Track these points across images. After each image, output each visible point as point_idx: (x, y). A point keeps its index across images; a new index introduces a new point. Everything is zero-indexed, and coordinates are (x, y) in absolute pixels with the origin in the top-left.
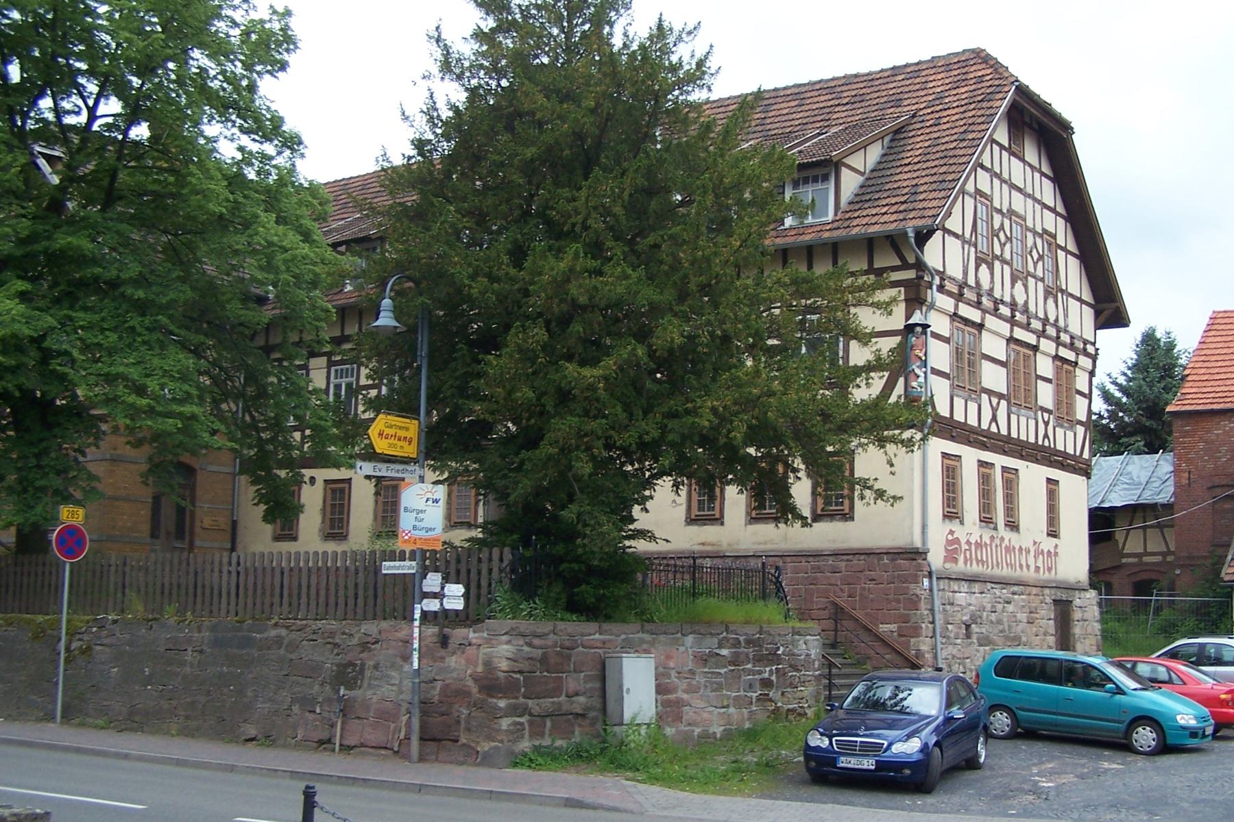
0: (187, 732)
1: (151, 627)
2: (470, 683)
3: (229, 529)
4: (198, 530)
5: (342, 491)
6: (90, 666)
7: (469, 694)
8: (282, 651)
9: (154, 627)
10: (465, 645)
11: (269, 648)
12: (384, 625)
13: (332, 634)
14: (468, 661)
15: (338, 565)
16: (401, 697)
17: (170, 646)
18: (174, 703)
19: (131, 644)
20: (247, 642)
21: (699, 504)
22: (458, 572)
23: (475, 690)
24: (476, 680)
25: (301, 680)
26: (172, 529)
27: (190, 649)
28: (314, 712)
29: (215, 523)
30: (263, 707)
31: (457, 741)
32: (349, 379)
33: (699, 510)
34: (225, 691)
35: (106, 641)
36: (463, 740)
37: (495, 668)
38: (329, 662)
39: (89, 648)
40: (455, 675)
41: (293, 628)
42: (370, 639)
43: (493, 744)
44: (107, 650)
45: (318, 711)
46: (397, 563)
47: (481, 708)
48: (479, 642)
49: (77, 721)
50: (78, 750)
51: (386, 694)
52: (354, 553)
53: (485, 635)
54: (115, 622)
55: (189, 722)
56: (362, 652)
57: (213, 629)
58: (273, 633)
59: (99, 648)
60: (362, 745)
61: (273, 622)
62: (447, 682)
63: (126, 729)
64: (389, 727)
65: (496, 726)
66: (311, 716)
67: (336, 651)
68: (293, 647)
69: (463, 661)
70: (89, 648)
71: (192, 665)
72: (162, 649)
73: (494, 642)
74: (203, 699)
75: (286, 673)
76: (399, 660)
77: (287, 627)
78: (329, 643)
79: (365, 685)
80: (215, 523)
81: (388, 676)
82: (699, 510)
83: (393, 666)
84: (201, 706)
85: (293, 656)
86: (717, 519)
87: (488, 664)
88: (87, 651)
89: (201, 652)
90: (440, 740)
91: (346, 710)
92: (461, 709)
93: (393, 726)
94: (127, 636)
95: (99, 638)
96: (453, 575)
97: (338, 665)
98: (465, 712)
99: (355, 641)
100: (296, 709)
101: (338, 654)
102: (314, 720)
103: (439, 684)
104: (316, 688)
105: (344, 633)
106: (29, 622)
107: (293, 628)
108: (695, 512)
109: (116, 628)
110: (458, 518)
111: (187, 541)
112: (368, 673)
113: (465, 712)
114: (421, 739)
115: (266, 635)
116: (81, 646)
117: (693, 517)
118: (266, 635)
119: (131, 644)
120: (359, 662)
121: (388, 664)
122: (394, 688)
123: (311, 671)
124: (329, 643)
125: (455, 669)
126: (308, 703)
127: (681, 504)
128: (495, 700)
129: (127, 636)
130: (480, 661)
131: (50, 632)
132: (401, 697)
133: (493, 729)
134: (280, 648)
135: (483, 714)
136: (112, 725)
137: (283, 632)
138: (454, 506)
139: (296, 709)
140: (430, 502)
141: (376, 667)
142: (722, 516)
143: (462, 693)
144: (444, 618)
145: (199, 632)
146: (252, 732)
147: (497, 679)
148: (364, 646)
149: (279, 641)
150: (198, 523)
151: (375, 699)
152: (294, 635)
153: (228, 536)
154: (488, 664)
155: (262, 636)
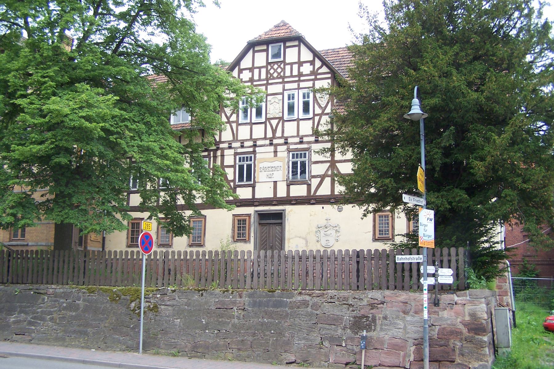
0: (60, 341)
1: (202, 294)
2: (461, 327)
3: (101, 241)
4: (89, 241)
5: (245, 220)
6: (157, 318)
7: (461, 333)
8: (309, 309)
9: (204, 294)
10: (452, 304)
11: (298, 308)
12: (387, 293)
13: (346, 299)
14: (457, 314)
15: (246, 258)
16: (407, 336)
17: (219, 306)
18: (228, 341)
19: (188, 305)
20: (279, 304)
21: (131, 239)
22: (449, 261)
23: (465, 331)
24: (465, 325)
25: (327, 327)
26: (77, 241)
27: (235, 308)
28: (341, 346)
29: (96, 238)
30: (299, 343)
31: (454, 362)
32: (303, 159)
33: (131, 242)
34: (268, 333)
35: (168, 303)
36: (458, 360)
37: (480, 318)
38: (347, 316)
39: (156, 307)
40: (449, 322)
41: (314, 295)
42: (376, 301)
43: (481, 363)
44: (170, 308)
45: (344, 345)
46: (408, 256)
47: (470, 341)
48: (464, 302)
49: (152, 351)
50: (84, 362)
51: (395, 334)
52: (210, 252)
53: (468, 298)
54: (174, 291)
55: (241, 353)
56: (372, 309)
57: (250, 296)
58: (300, 298)
59: (163, 307)
60: (380, 365)
61: (298, 291)
62: (443, 326)
63: (195, 357)
64: (400, 354)
65: (483, 352)
66: (339, 348)
67: (351, 309)
68: (316, 306)
69: (453, 314)
70: (156, 307)
71: (238, 318)
72: (213, 308)
73: (477, 302)
74: (250, 338)
75: (314, 322)
76: (401, 313)
77: (310, 295)
78: (345, 304)
79: (378, 328)
80: (96, 238)
81: (395, 323)
82: (131, 242)
83: (397, 317)
84: (249, 343)
85: (318, 312)
86: (390, 239)
87: (473, 315)
88: (155, 308)
89: (244, 309)
90: (440, 361)
91: (368, 344)
92: (456, 342)
93: (402, 353)
94: (186, 300)
95: (164, 301)
96: (445, 262)
97: (355, 317)
98: (459, 344)
99: (365, 302)
100: (326, 344)
101: (353, 311)
102: (342, 350)
103: (438, 328)
104: (340, 331)
105: (355, 298)
106: (106, 291)
107: (314, 295)
108: (377, 236)
109: (176, 295)
110: (161, 241)
111: (83, 247)
112: (378, 322)
113: (459, 344)
114: (430, 361)
115: (294, 299)
116: (149, 306)
117: (377, 238)
118: (294, 299)
119: (188, 305)
120: (371, 315)
121: (394, 317)
122: (400, 330)
123: (335, 321)
124: (345, 304)
125: (448, 319)
126: (336, 341)
127: (370, 232)
128: (480, 337)
129: (186, 300)
130: (467, 314)
131: (123, 297)
132: (407, 336)
133: (480, 354)
134: (307, 307)
135: (472, 345)
136: (180, 354)
137: (308, 298)
138: (160, 235)
139: (326, 344)
140: (429, 220)
141: (385, 318)
142: (172, 244)
143: (456, 333)
144: (444, 288)
145: (241, 297)
146: (293, 359)
147: (482, 324)
148: (372, 306)
149: (305, 304)
150: (89, 238)
151: (387, 337)
152: (316, 300)
153: (101, 245)
154: (473, 315)
155: (291, 300)
